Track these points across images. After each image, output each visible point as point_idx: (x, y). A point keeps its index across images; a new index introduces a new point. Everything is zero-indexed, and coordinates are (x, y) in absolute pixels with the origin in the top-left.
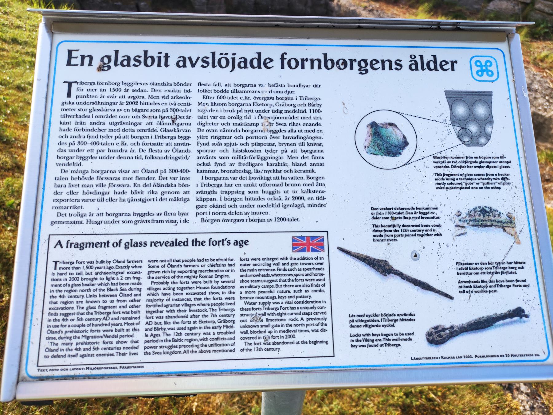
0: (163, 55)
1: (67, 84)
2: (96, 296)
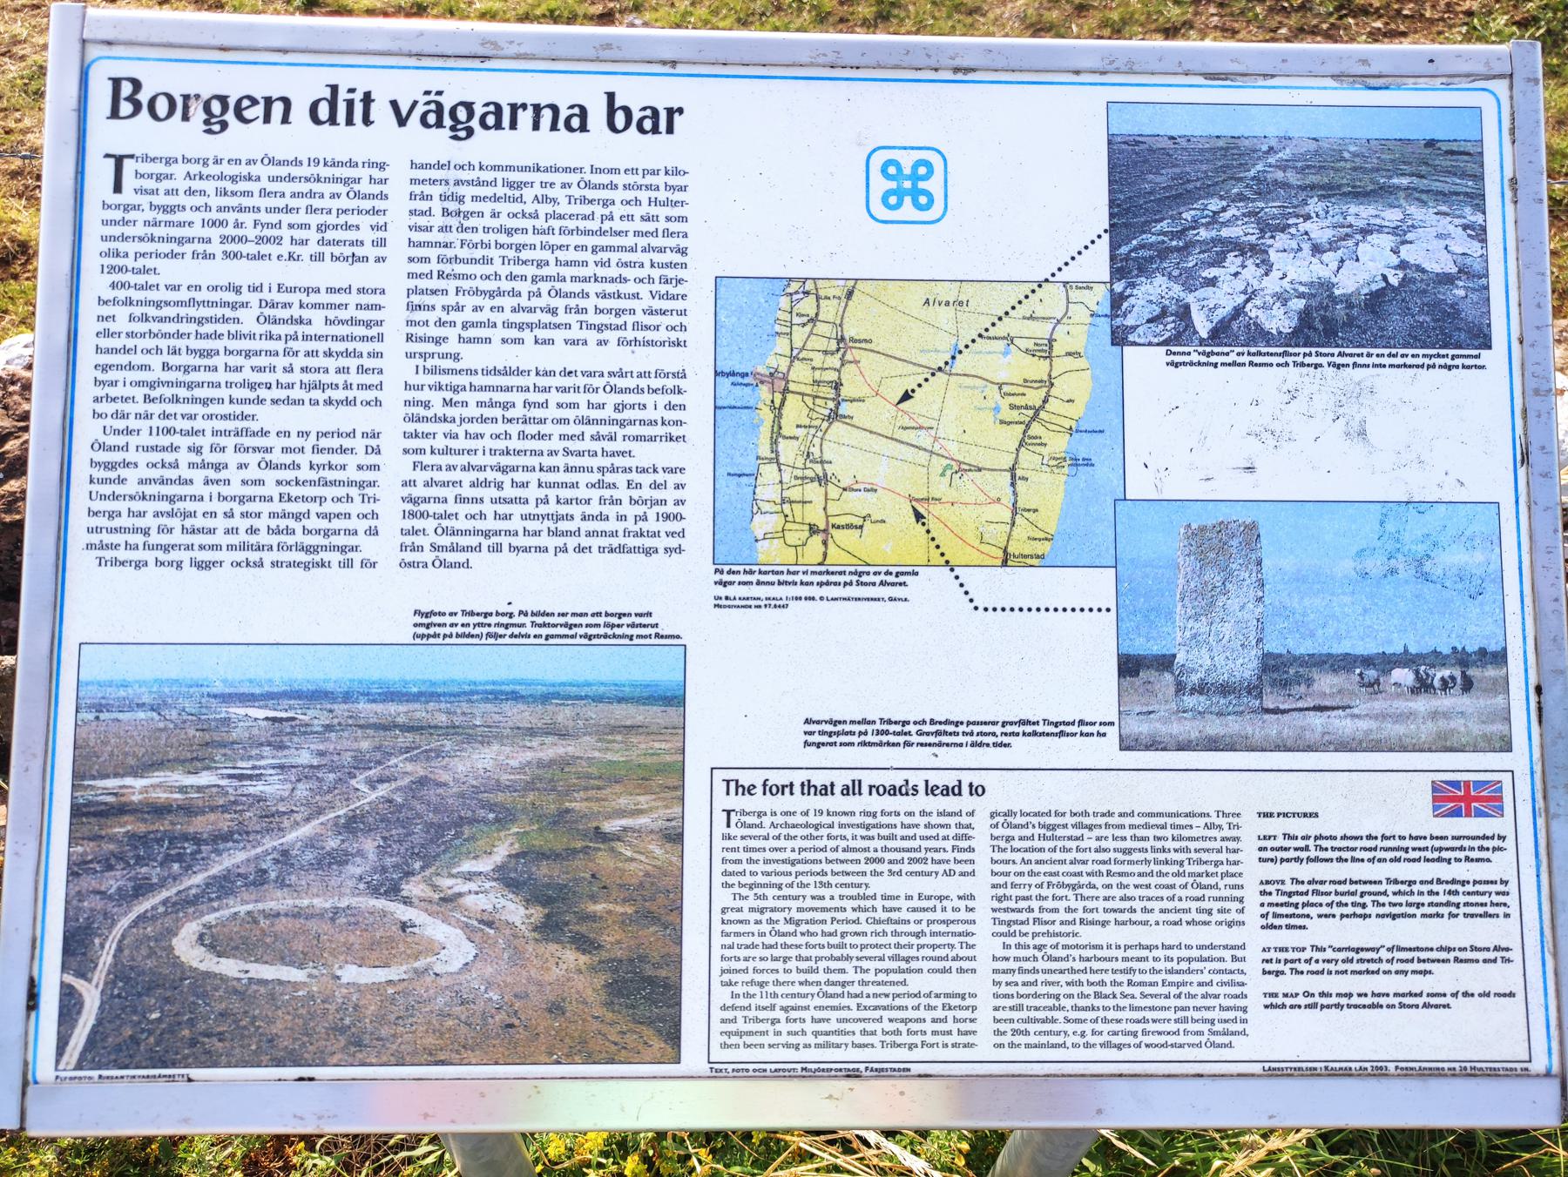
0: (358, 96)
1: (112, 161)
2: (1219, 911)
